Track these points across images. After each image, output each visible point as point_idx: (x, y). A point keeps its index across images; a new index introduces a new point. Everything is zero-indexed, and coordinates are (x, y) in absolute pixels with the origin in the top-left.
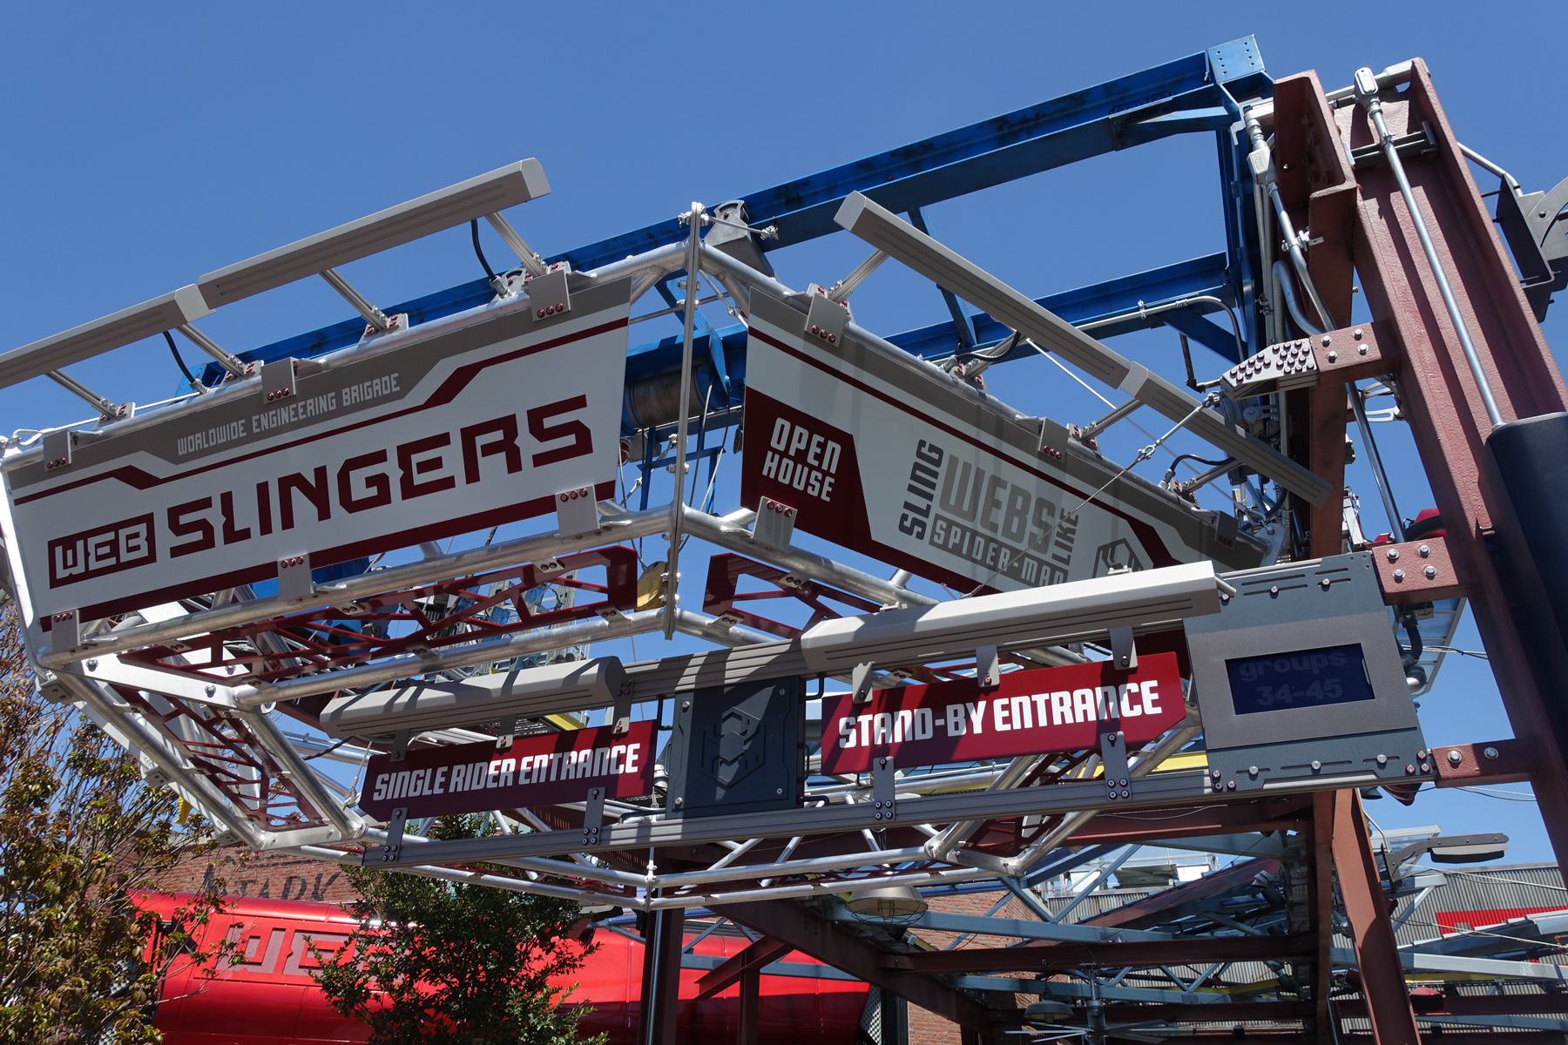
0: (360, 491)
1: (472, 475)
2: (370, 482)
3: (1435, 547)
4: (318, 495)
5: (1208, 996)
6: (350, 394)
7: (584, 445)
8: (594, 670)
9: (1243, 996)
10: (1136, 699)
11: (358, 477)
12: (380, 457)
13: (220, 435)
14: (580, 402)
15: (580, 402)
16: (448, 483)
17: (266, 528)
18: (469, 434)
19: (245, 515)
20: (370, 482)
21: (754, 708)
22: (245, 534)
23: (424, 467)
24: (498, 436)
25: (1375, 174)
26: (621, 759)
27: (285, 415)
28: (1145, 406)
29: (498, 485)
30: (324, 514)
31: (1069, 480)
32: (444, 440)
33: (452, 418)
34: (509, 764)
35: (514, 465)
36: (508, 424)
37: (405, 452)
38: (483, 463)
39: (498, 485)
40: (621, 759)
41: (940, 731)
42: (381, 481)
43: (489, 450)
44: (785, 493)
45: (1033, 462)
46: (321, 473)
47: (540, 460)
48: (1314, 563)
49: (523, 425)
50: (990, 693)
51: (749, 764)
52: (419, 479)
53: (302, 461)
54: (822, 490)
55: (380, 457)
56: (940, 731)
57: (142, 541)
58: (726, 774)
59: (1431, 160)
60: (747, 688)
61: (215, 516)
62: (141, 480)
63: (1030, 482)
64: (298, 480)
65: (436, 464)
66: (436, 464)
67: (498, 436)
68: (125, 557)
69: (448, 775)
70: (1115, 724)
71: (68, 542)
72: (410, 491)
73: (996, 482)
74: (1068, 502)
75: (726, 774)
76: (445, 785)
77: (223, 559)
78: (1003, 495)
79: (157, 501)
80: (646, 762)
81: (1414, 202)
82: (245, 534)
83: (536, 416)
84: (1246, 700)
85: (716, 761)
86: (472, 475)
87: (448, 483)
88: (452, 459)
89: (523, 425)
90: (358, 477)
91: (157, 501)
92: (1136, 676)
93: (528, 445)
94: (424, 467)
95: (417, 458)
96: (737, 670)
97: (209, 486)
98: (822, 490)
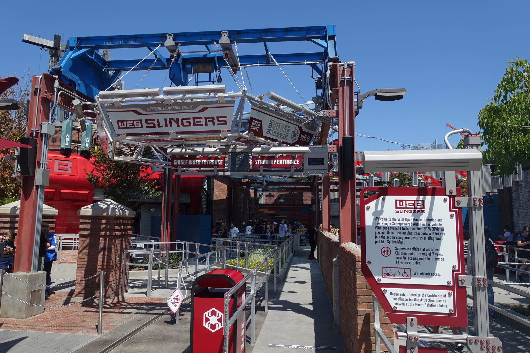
0: (185, 123)
1: (206, 124)
2: (187, 122)
3: (335, 146)
4: (177, 122)
5: (290, 180)
6: (183, 107)
7: (226, 123)
8: (218, 150)
9: (299, 180)
10: (296, 162)
11: (185, 121)
12: (189, 119)
13: (156, 109)
14: (226, 117)
15: (226, 117)
16: (202, 125)
17: (166, 126)
18: (206, 118)
19: (162, 123)
20: (187, 122)
21: (241, 157)
22: (162, 126)
23: (197, 122)
24: (211, 119)
25: (342, 82)
26: (219, 162)
27: (170, 108)
28: (312, 320)
29: (210, 127)
30: (178, 126)
31: (290, 121)
32: (201, 118)
33: (203, 115)
34: (199, 161)
35: (214, 124)
36: (213, 118)
37: (194, 119)
38: (208, 123)
39: (210, 127)
40: (219, 162)
41: (269, 163)
42: (190, 123)
43: (209, 121)
44: (253, 131)
45: (286, 120)
46: (178, 119)
47: (218, 124)
48: (321, 146)
49: (216, 118)
50: (277, 159)
51: (241, 165)
52: (196, 123)
53: (175, 117)
54: (257, 129)
55: (189, 119)
56: (269, 163)
57: (140, 124)
58: (237, 166)
59: (350, 83)
60: (240, 153)
61: (156, 122)
62: (139, 113)
63: (284, 123)
64: (173, 119)
65: (200, 122)
66: (200, 122)
67: (211, 119)
68: (136, 126)
69: (188, 161)
70: (293, 165)
71: (122, 122)
72: (195, 125)
73: (280, 124)
74: (290, 125)
75: (237, 166)
76: (188, 163)
77: (157, 130)
78: (281, 126)
79: (143, 118)
80: (224, 162)
81: (346, 88)
82: (162, 126)
83: (218, 118)
84: (309, 164)
85: (235, 164)
86: (206, 124)
87: (202, 125)
88: (203, 121)
89: (216, 118)
90: (185, 121)
91: (143, 118)
92: (297, 159)
93: (216, 122)
94: (197, 122)
95: (196, 120)
96: (238, 150)
97: (155, 117)
98: (257, 129)
